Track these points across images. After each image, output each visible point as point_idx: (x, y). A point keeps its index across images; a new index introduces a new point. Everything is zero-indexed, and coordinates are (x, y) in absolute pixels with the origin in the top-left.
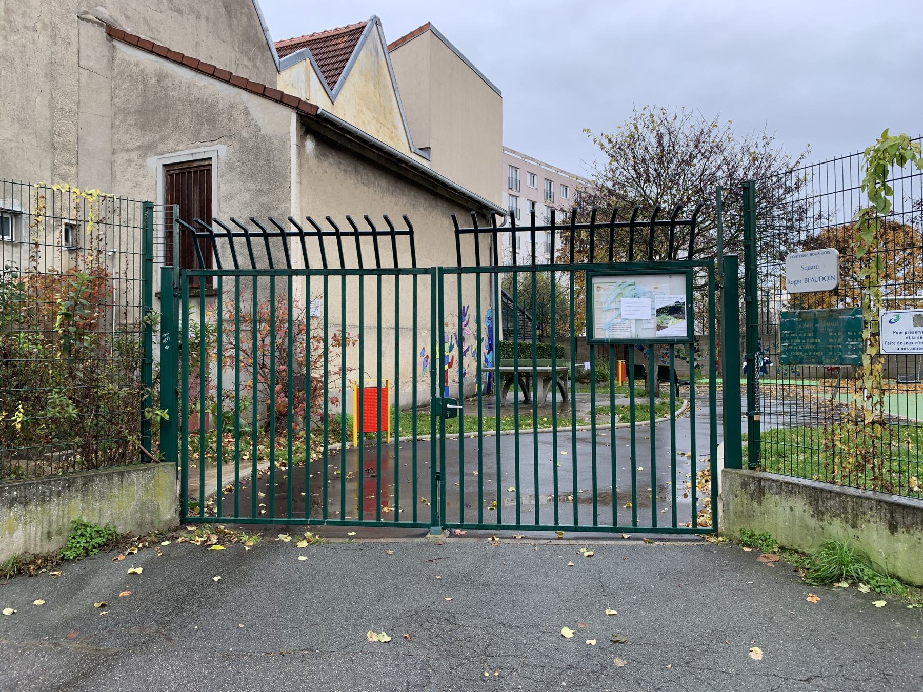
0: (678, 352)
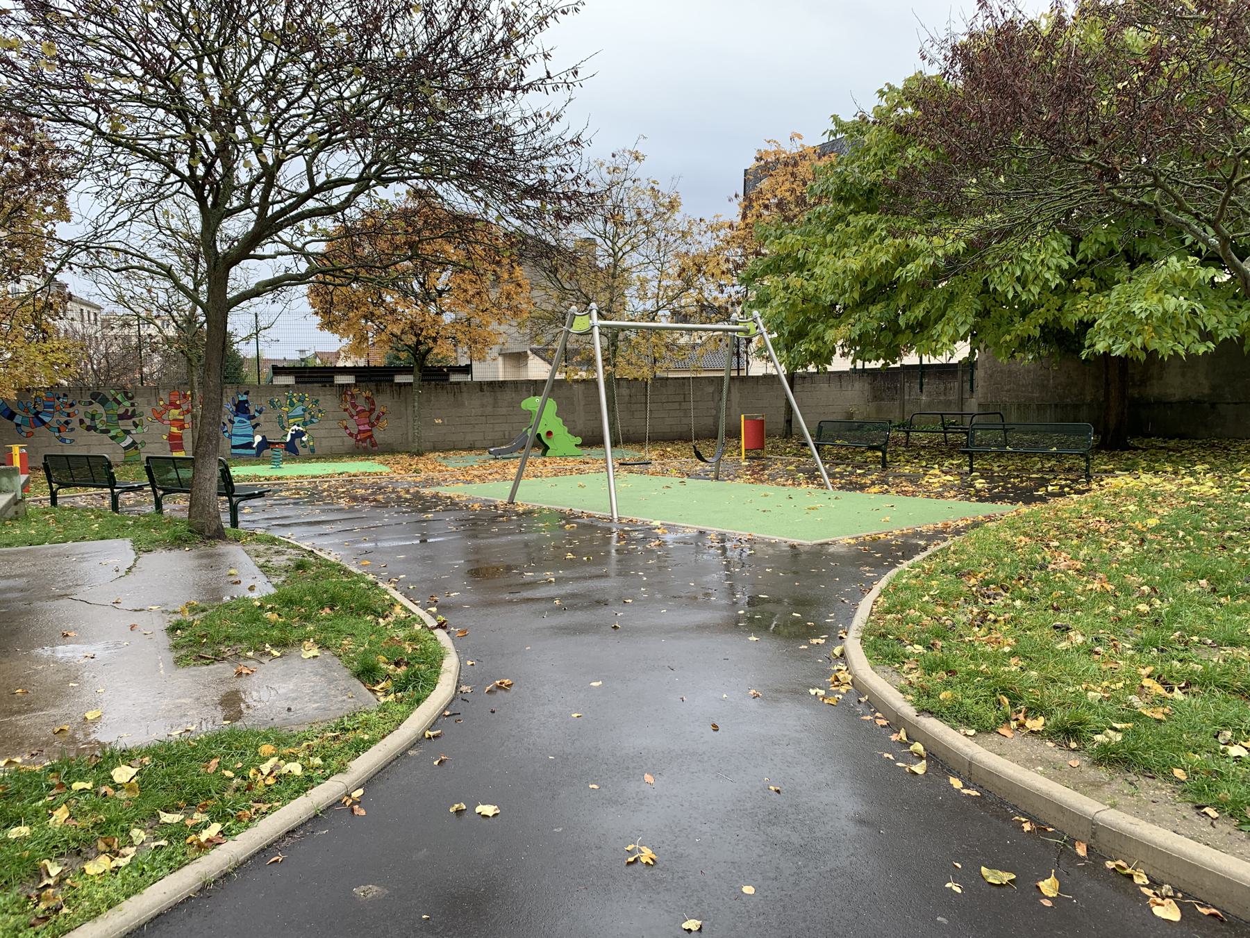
0: (93, 418)
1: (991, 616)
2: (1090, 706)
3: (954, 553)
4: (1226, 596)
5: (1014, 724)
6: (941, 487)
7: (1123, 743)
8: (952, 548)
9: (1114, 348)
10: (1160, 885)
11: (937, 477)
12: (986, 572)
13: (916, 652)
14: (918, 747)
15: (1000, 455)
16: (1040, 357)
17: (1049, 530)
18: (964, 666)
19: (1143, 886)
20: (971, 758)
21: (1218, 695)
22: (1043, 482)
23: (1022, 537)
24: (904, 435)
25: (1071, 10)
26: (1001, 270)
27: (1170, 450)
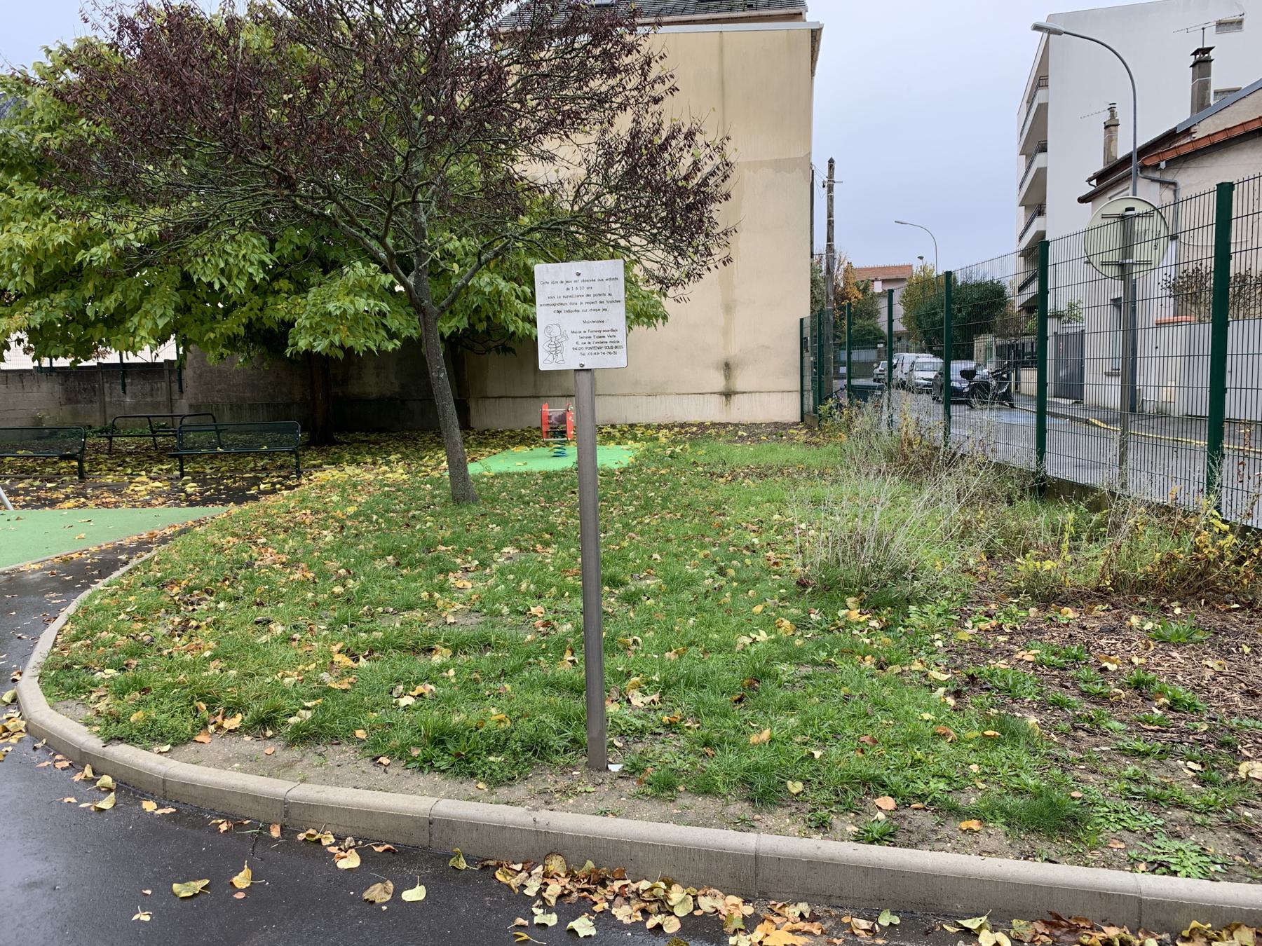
1: (193, 623)
2: (285, 692)
3: (158, 563)
4: (406, 567)
5: (212, 728)
6: (148, 494)
7: (312, 720)
8: (156, 559)
9: (315, 344)
10: (343, 840)
11: (143, 485)
12: (191, 578)
13: (107, 677)
14: (107, 780)
15: (215, 456)
16: (251, 358)
17: (257, 528)
18: (157, 678)
19: (330, 846)
20: (165, 775)
21: (394, 655)
22: (256, 481)
23: (230, 538)
24: (107, 441)
25: (241, 11)
26: (204, 261)
27: (370, 443)
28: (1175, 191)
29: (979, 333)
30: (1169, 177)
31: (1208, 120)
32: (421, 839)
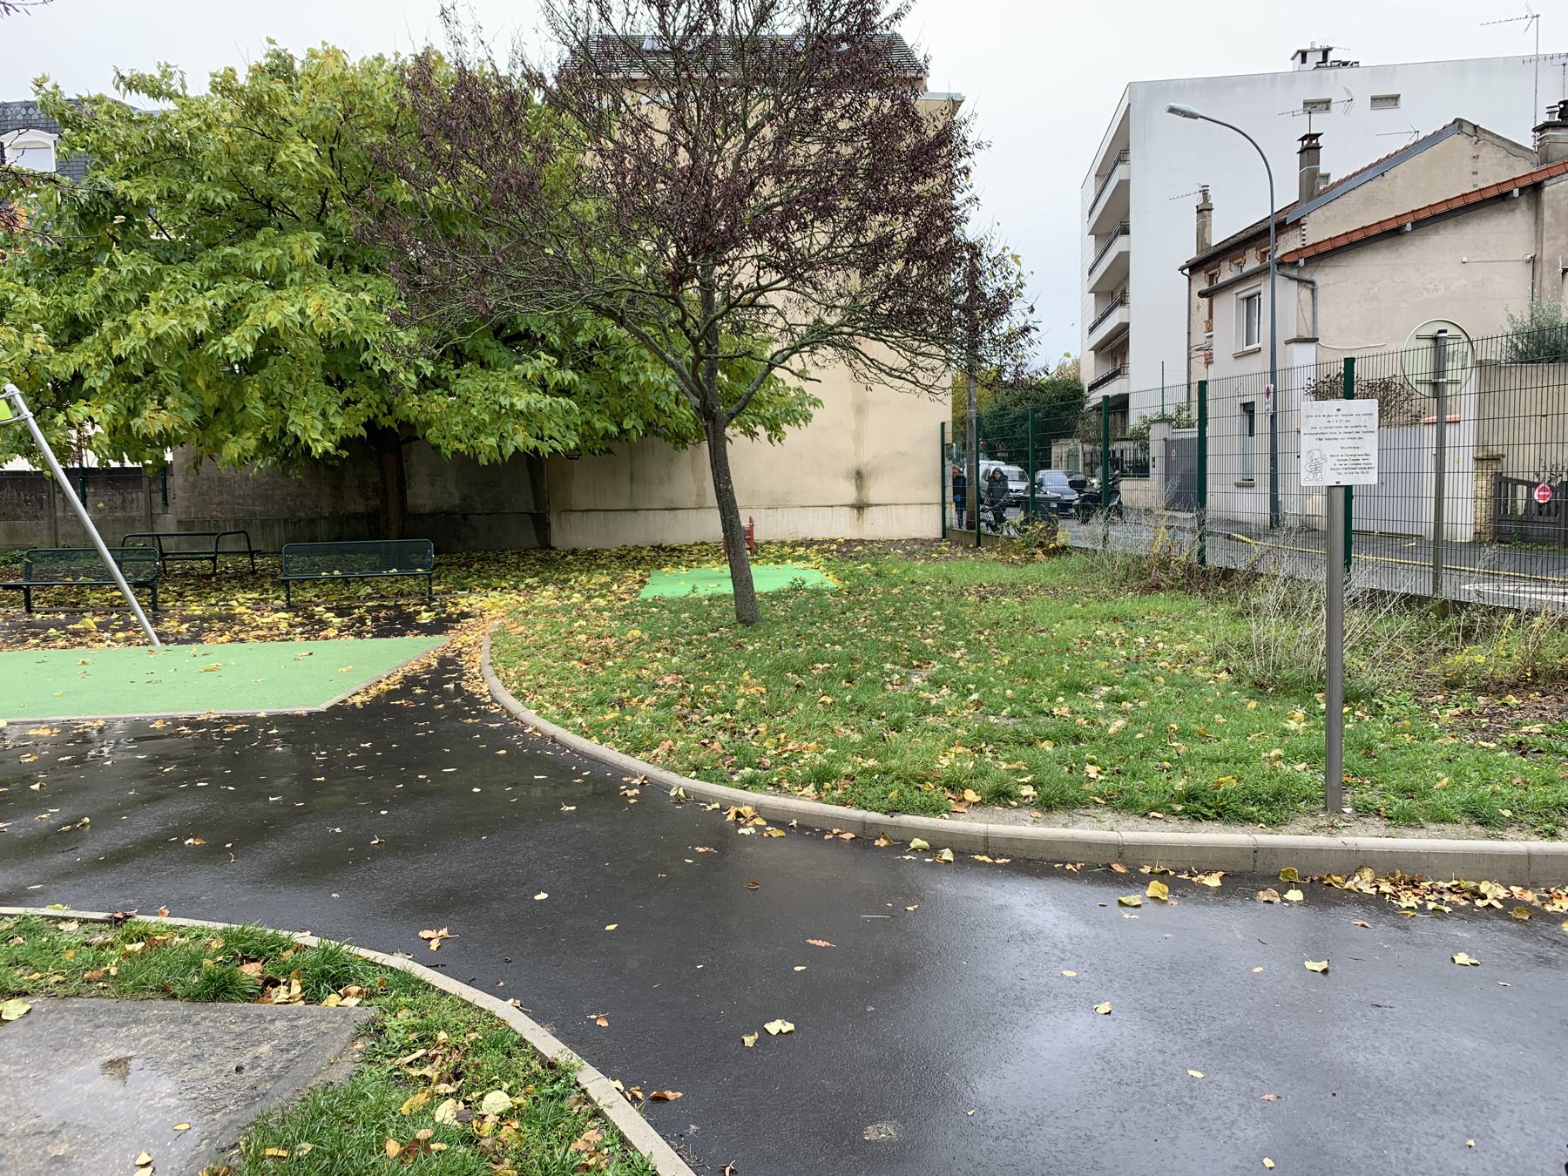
28: (1313, 291)
29: (1058, 437)
30: (1307, 277)
31: (1318, 212)
32: (1246, 865)
